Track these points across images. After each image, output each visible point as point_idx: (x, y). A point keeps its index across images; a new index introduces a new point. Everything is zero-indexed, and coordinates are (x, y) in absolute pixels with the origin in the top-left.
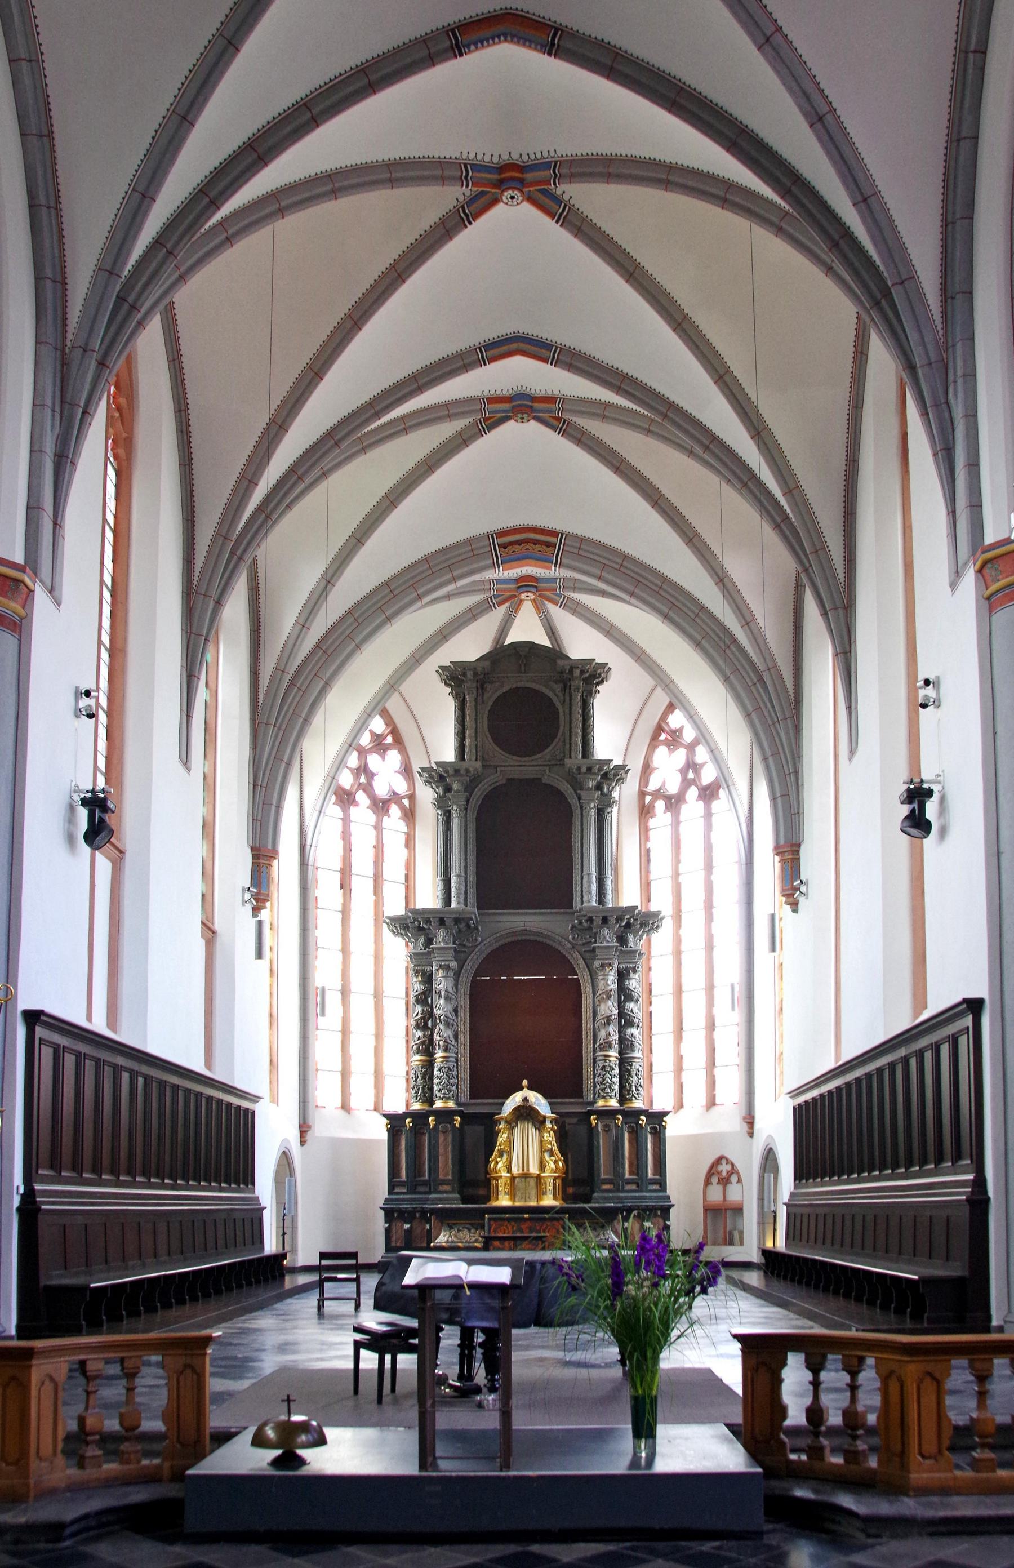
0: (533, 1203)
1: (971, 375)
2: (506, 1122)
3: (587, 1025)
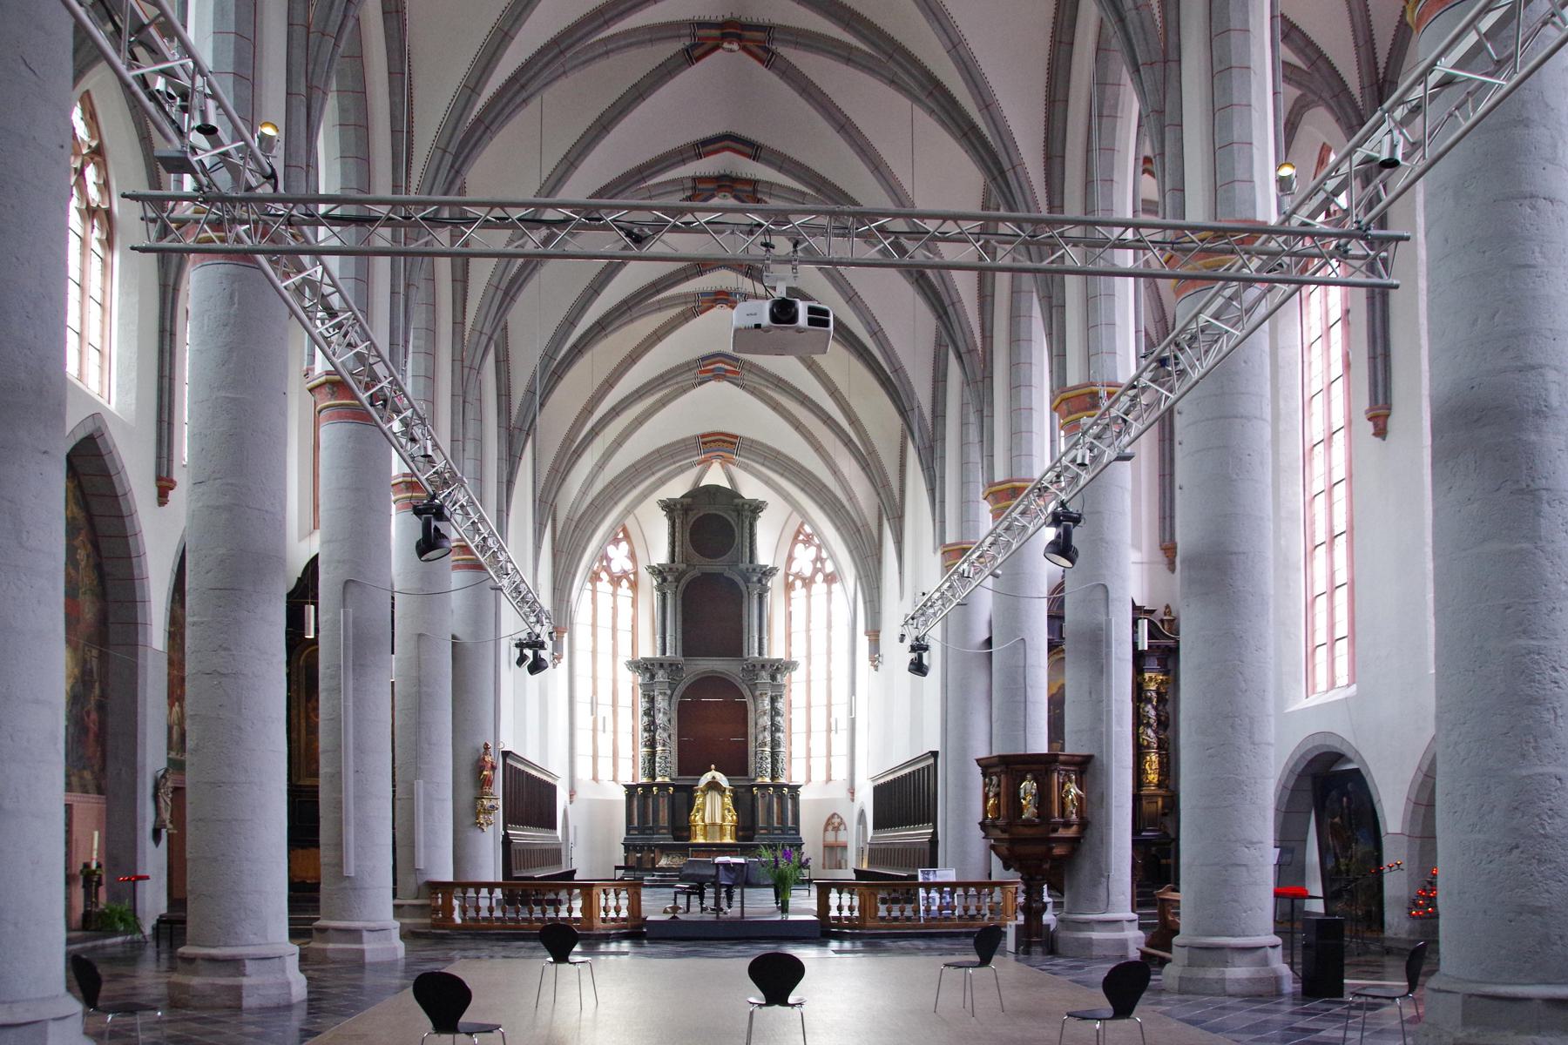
0: (718, 842)
1: (943, 457)
2: (702, 791)
3: (751, 730)
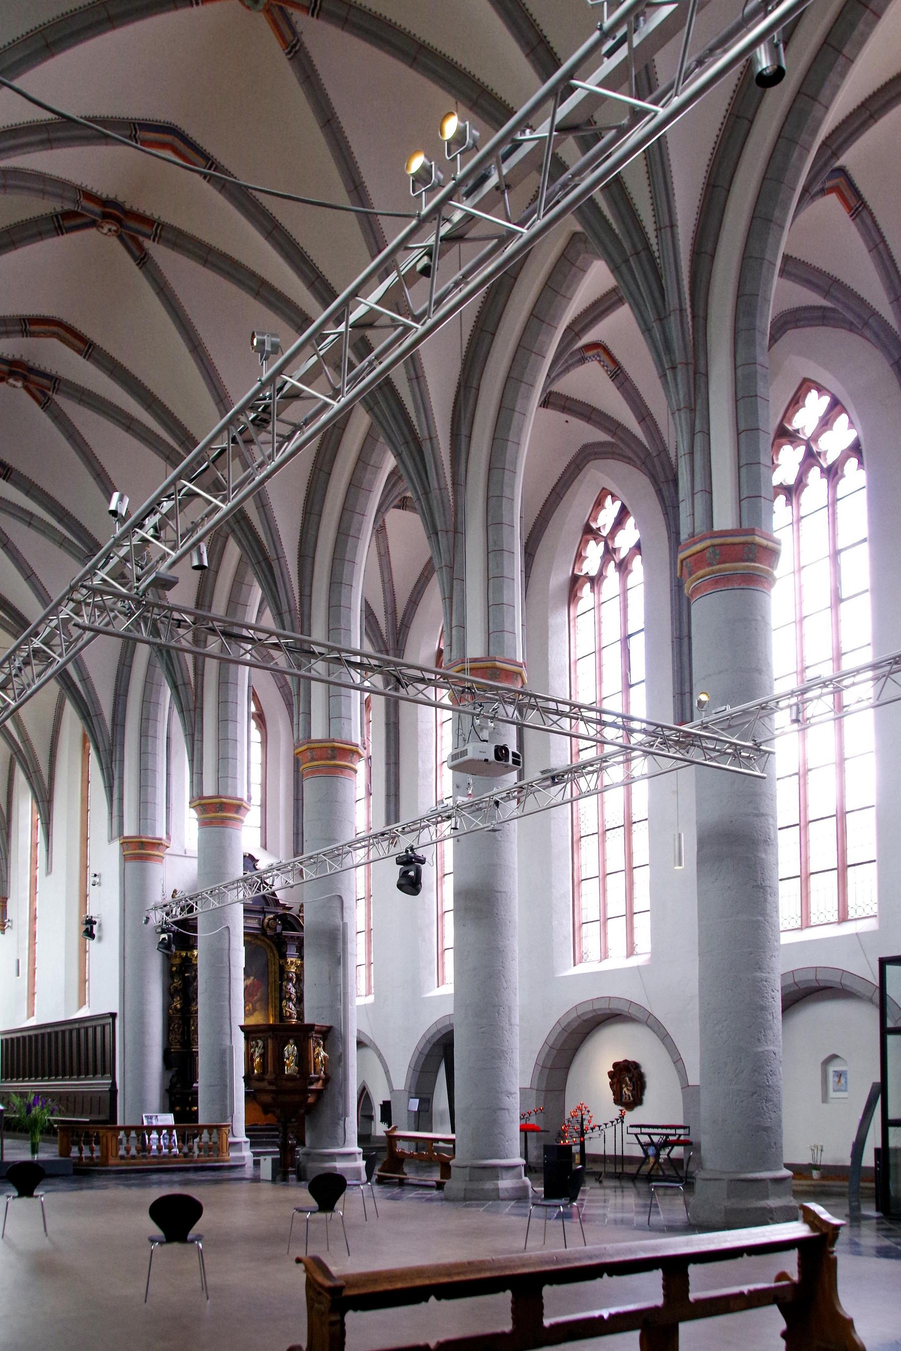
1: (122, 761)
